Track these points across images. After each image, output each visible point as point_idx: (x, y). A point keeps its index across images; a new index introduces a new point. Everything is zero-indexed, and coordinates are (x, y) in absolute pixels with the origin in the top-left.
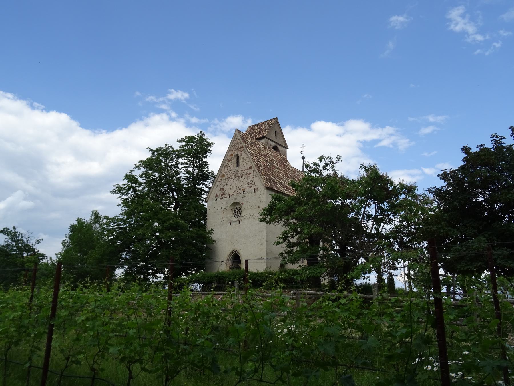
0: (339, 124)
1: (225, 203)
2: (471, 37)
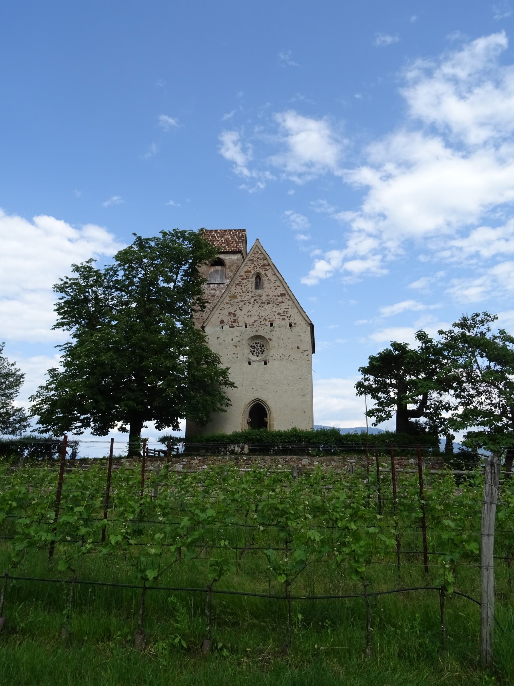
0: (74, 225)
1: (239, 335)
2: (238, 168)
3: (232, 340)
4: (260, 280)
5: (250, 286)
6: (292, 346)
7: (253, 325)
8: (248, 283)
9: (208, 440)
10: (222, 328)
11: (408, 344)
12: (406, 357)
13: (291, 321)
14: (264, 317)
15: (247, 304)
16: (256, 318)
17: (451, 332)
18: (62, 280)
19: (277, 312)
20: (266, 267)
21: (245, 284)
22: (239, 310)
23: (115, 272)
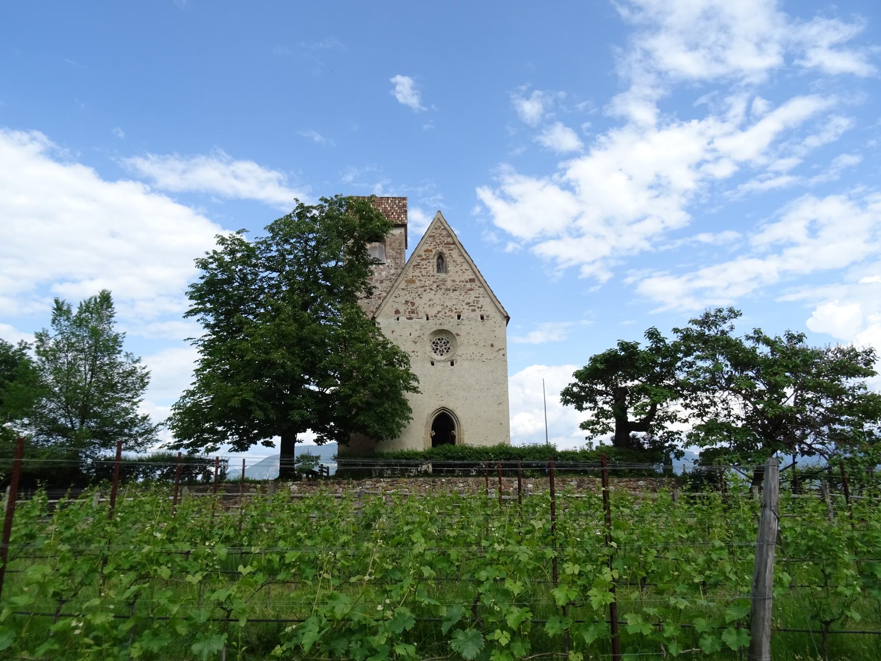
4: (443, 261)
9: (396, 457)
13: (482, 313)
16: (439, 308)
18: (207, 253)
22: (418, 298)
23: (269, 246)
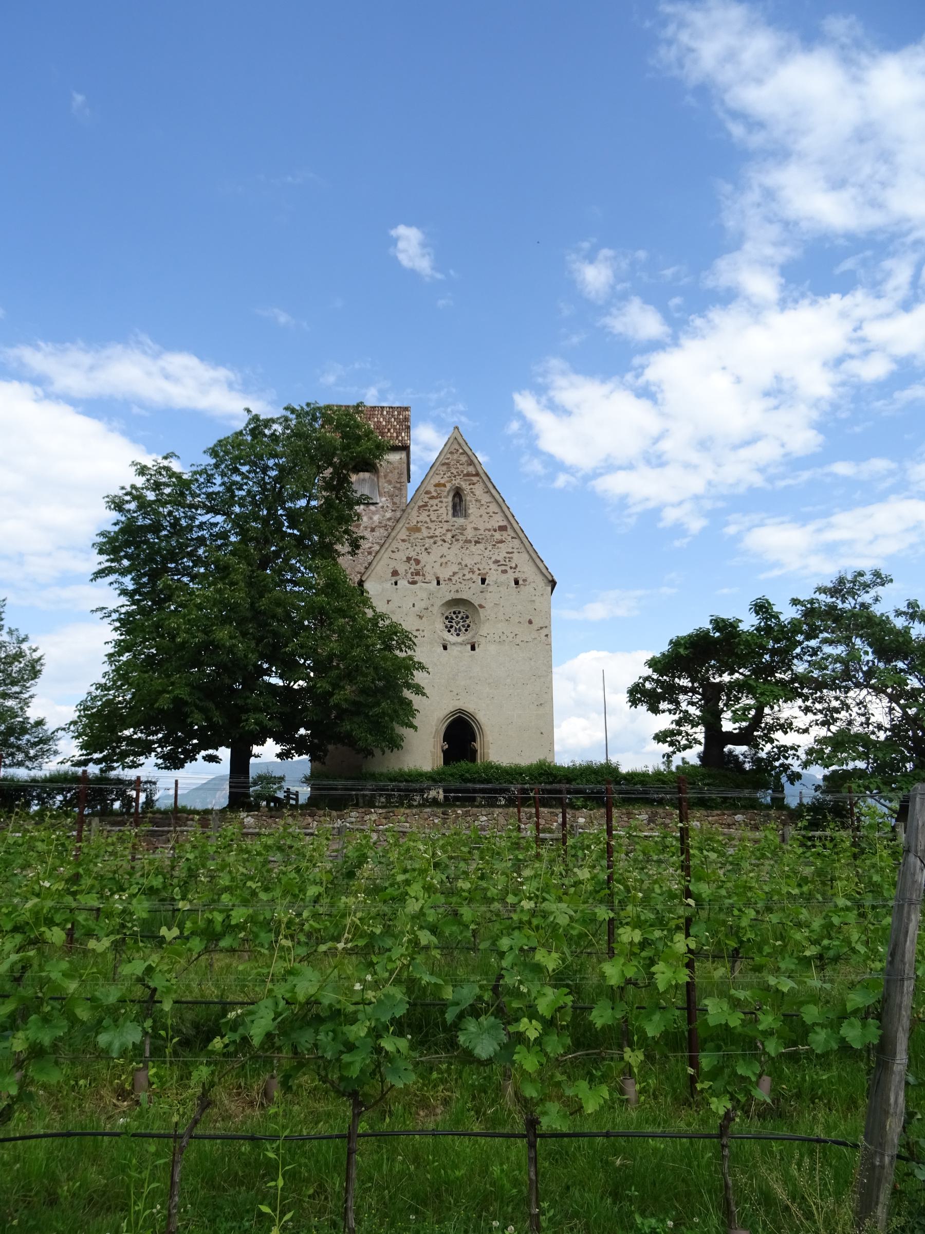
3: (414, 605)
4: (461, 500)
5: (443, 510)
6: (521, 620)
7: (450, 579)
8: (440, 505)
10: (396, 583)
11: (740, 621)
12: (739, 644)
13: (517, 575)
14: (469, 566)
15: (440, 543)
16: (455, 568)
17: (811, 602)
19: (493, 559)
20: (473, 478)
21: (435, 508)
22: (424, 553)
23: (209, 479)
